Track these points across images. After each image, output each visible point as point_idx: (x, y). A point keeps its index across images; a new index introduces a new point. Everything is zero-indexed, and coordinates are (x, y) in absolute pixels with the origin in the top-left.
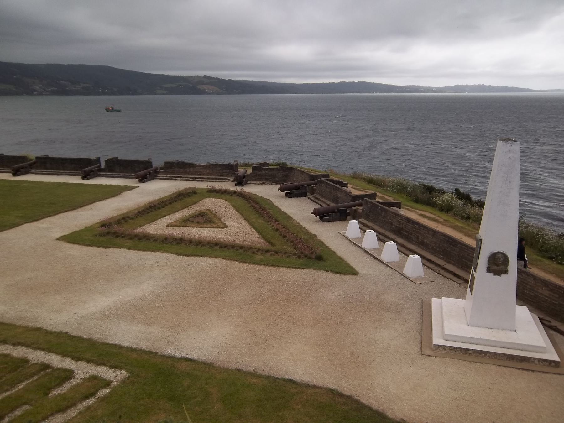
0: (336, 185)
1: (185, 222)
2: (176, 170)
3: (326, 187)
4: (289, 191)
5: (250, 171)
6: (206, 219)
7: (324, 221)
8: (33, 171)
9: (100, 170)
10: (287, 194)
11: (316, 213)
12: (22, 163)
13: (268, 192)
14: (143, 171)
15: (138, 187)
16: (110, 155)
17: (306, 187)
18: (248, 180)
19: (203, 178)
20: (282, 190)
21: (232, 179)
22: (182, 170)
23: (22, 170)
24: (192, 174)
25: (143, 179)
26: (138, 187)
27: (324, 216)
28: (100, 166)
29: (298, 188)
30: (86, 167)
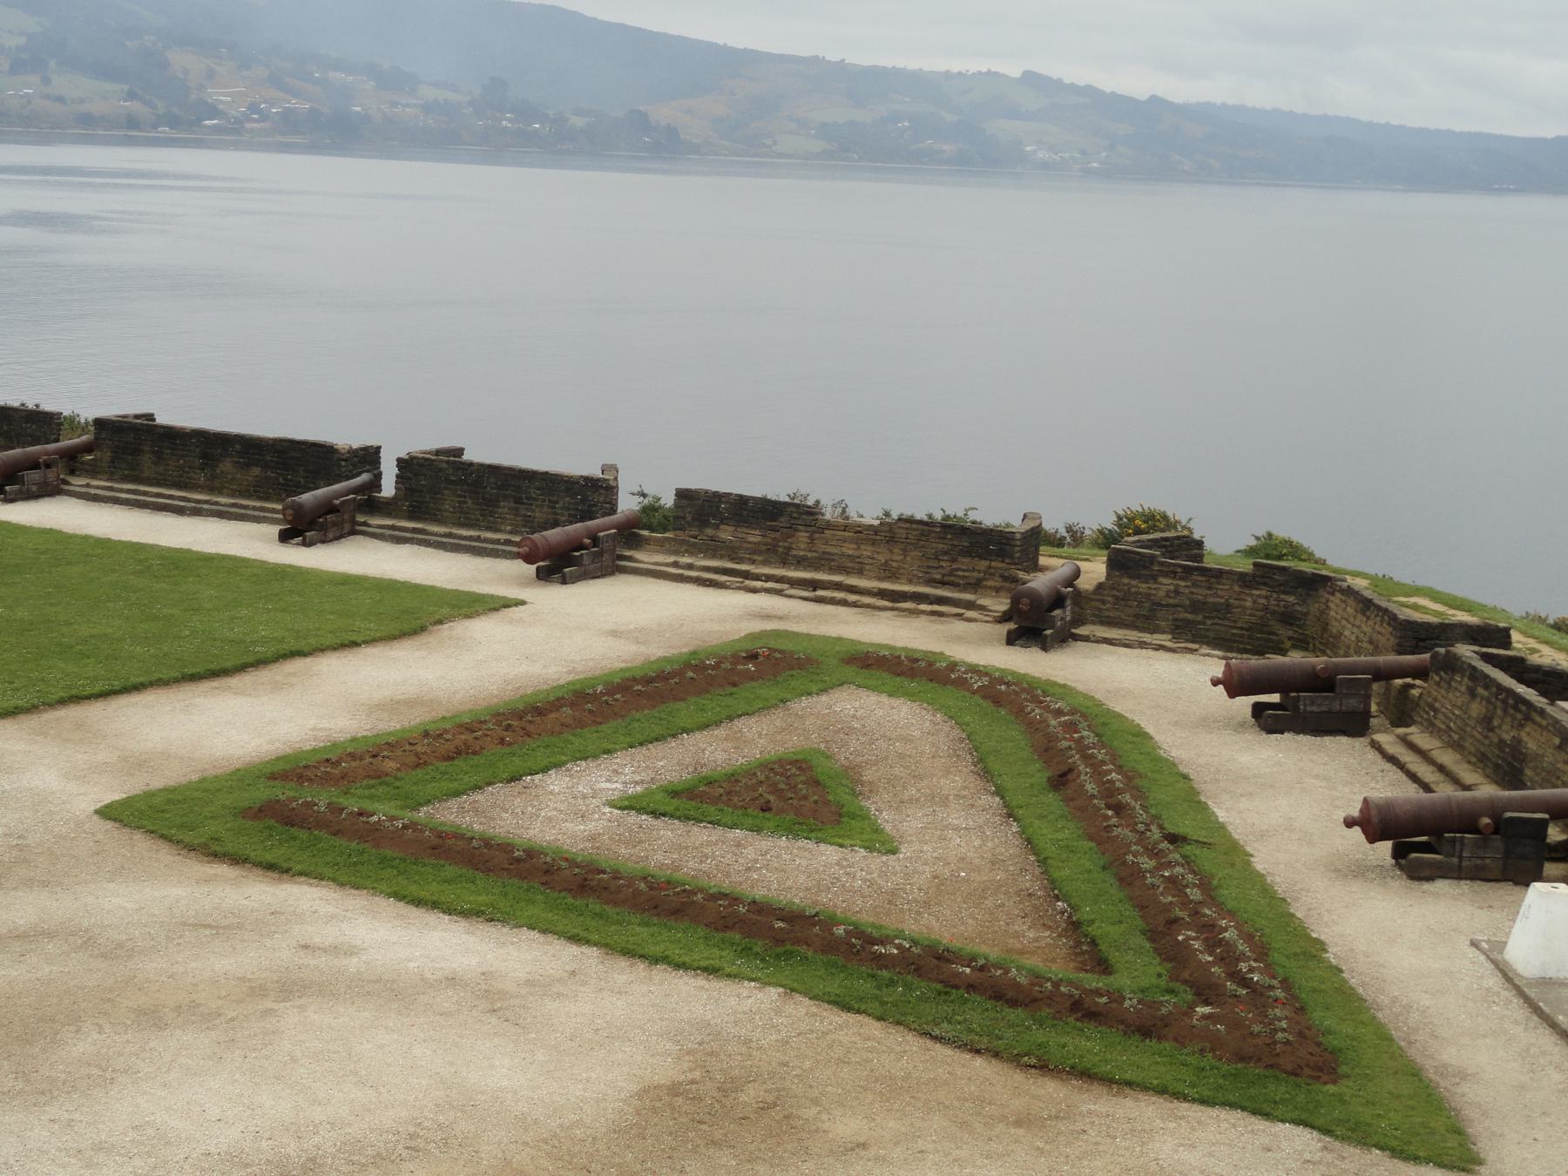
0: (1521, 689)
1: (699, 799)
2: (726, 534)
3: (1472, 693)
4: (1275, 698)
5: (1095, 570)
6: (800, 796)
7: (1418, 874)
8: (78, 482)
9: (369, 502)
10: (1258, 709)
11: (1375, 823)
12: (36, 441)
13: (1161, 690)
14: (562, 524)
15: (523, 603)
16: (423, 442)
17: (1368, 683)
18: (1079, 621)
19: (852, 590)
20: (1235, 685)
21: (1001, 605)
22: (754, 536)
23: (33, 476)
24: (801, 563)
25: (558, 566)
26: (523, 603)
27: (1419, 843)
28: (375, 484)
29: (1321, 683)
30: (304, 482)
